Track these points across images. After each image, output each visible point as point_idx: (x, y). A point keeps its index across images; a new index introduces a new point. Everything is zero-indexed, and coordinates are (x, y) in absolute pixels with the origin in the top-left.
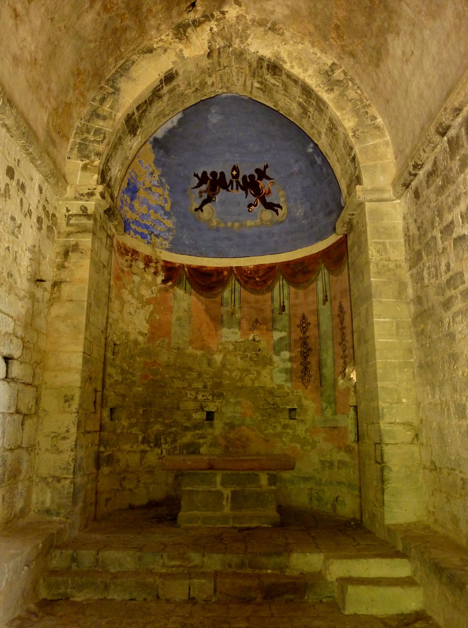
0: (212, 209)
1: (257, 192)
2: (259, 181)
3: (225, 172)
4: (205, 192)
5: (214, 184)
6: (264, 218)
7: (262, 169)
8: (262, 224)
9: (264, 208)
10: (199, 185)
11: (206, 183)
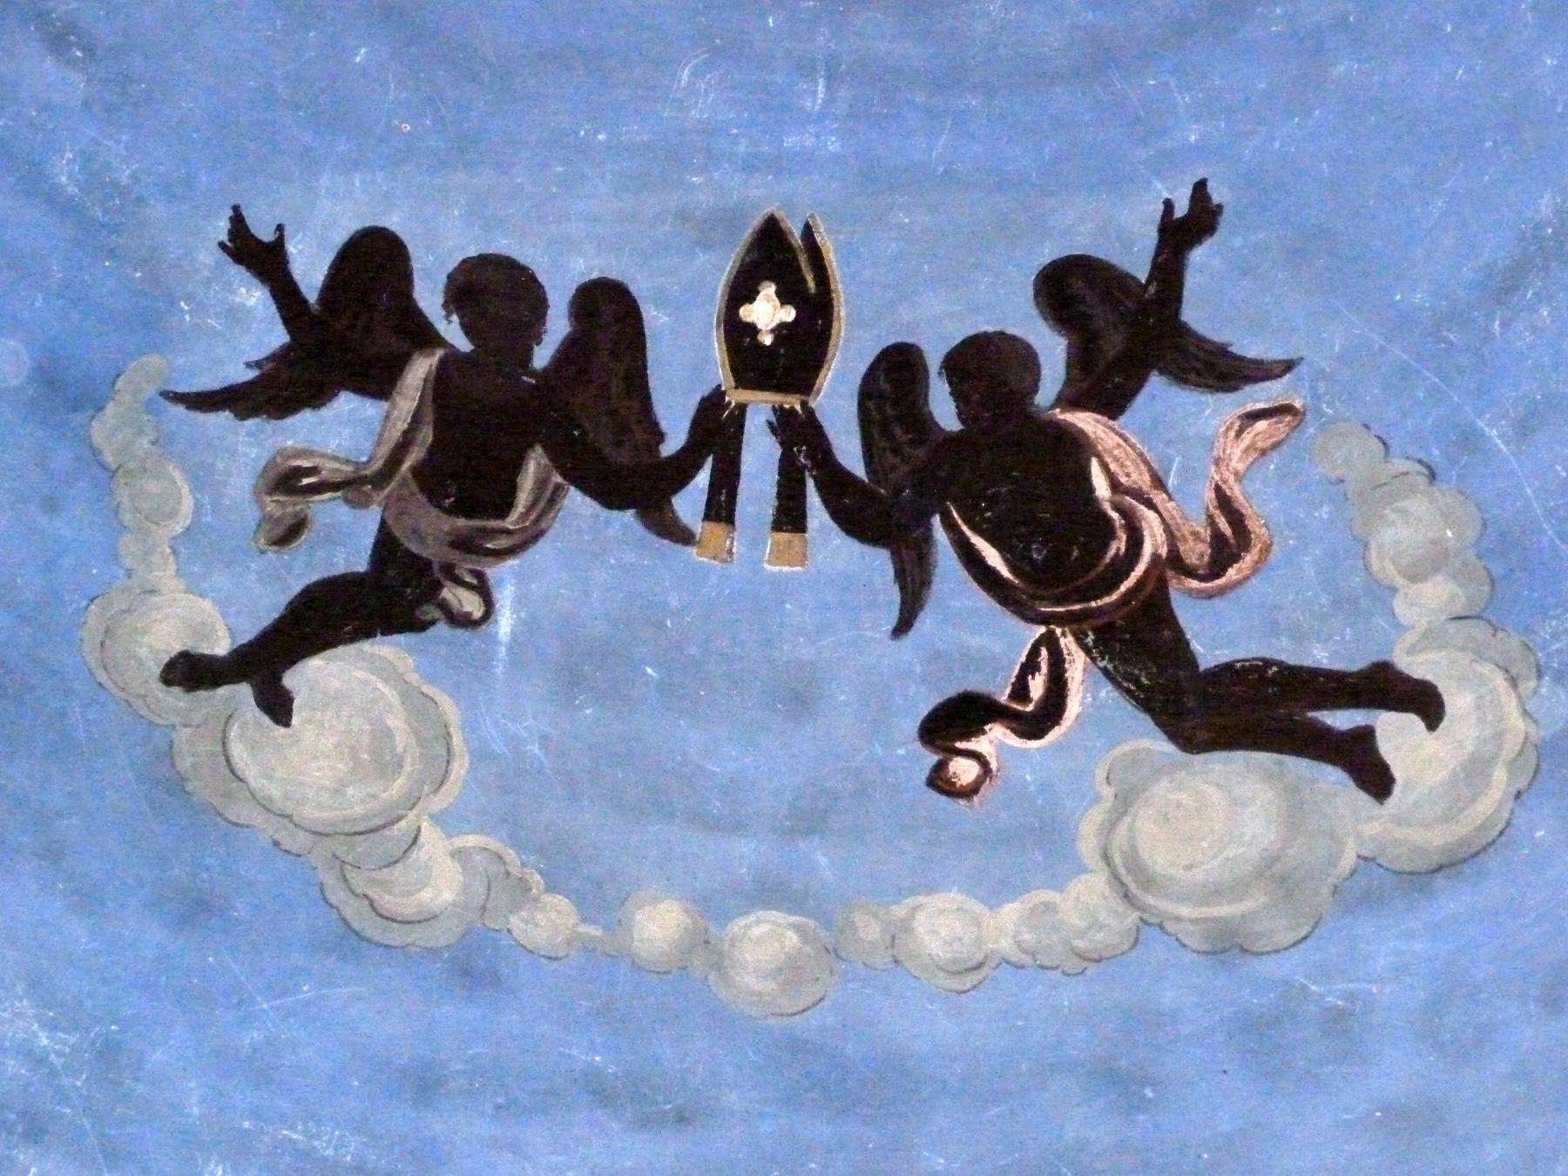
0: (419, 707)
1: (1059, 547)
2: (1086, 421)
3: (639, 287)
4: (353, 486)
5: (487, 415)
6: (1160, 857)
7: (1137, 261)
8: (1151, 925)
9: (1160, 745)
10: (276, 391)
11: (377, 380)
